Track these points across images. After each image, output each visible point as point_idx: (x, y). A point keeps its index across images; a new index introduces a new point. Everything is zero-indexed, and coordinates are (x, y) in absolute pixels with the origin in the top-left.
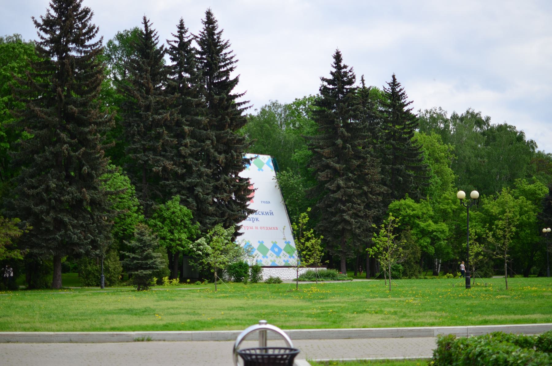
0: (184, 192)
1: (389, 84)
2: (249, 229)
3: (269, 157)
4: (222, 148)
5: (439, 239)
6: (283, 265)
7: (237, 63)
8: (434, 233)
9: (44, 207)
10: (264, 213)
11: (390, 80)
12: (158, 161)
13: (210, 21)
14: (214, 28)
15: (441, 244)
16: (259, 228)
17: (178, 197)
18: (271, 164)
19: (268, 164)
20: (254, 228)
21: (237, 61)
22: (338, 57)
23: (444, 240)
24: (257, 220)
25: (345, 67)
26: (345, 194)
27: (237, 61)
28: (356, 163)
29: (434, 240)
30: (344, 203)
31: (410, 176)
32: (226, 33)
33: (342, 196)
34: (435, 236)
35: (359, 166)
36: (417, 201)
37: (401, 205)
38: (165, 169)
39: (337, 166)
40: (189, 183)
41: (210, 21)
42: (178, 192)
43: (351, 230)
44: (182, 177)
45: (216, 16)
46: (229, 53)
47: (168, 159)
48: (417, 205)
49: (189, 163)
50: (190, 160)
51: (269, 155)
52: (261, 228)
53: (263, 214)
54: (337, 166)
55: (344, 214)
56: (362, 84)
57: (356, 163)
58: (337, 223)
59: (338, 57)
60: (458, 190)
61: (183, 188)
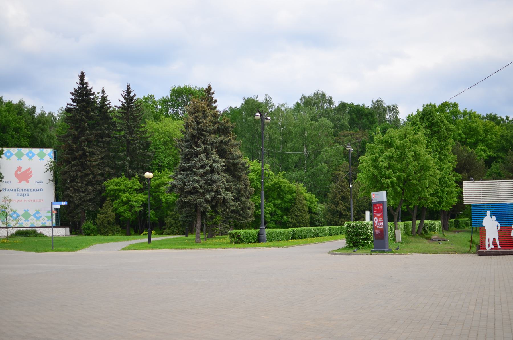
16: (27, 201)
24: (28, 195)
52: (29, 201)
53: (34, 190)
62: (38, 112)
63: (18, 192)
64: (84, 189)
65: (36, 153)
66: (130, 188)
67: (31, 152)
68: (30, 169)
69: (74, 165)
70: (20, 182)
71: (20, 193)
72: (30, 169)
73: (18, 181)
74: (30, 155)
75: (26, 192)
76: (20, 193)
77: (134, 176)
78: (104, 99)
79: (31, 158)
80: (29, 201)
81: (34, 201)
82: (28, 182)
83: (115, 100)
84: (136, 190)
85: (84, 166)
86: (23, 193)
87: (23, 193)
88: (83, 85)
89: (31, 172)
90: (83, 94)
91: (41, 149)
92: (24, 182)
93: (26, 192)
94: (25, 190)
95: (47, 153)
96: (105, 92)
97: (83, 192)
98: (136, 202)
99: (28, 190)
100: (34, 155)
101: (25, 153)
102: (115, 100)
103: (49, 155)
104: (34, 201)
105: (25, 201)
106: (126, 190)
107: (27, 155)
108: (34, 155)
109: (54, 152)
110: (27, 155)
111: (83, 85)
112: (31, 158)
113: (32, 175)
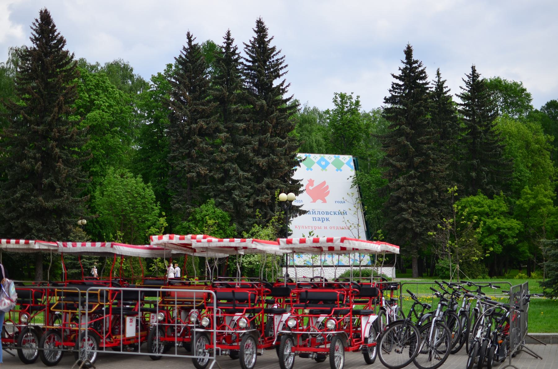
0: (222, 195)
1: (468, 76)
2: (317, 229)
3: (351, 157)
4: (265, 152)
5: (507, 237)
6: (302, 264)
7: (287, 68)
8: (501, 231)
9: (13, 214)
10: (337, 213)
11: (470, 71)
12: (194, 167)
13: (261, 29)
14: (265, 36)
15: (509, 242)
16: (328, 228)
17: (213, 201)
18: (352, 164)
19: (348, 163)
20: (323, 228)
21: (287, 66)
22: (409, 52)
23: (513, 237)
24: (327, 220)
25: (416, 62)
26: (406, 192)
27: (287, 66)
28: (417, 160)
29: (502, 238)
30: (406, 201)
31: (483, 170)
32: (276, 39)
33: (403, 194)
34: (503, 233)
35: (422, 162)
36: (491, 197)
37: (468, 201)
38: (199, 174)
39: (398, 164)
40: (227, 187)
41: (261, 29)
42: (215, 196)
43: (412, 228)
44: (222, 181)
45: (267, 24)
46: (281, 59)
47: (204, 166)
48: (489, 201)
49: (226, 167)
50: (227, 165)
51: (350, 155)
52: (331, 228)
53: (335, 213)
54: (398, 164)
55: (404, 213)
56: (437, 78)
57: (417, 160)
58: (399, 222)
59: (409, 52)
60: (280, 193)
61: (222, 192)
62: (301, 108)
63: (314, 216)
64: (426, 212)
65: (330, 161)
66: (495, 210)
67: (323, 159)
68: (324, 183)
69: (411, 177)
70: (314, 201)
71: (317, 216)
72: (324, 183)
73: (312, 200)
74: (323, 163)
75: (325, 216)
76: (317, 216)
77: (498, 194)
78: (440, 86)
79: (324, 168)
80: (331, 228)
81: (337, 228)
82: (325, 201)
83: (456, 89)
84: (502, 213)
85: (424, 177)
86: (321, 216)
87: (321, 216)
88: (411, 65)
89: (327, 187)
90: (411, 75)
91: (337, 156)
92: (319, 201)
93: (325, 216)
94: (323, 213)
95: (345, 162)
96: (441, 76)
97: (425, 216)
98: (509, 229)
99: (327, 213)
100: (327, 163)
101: (316, 161)
102: (456, 89)
103: (348, 163)
104: (337, 228)
105: (325, 228)
106: (490, 213)
107: (319, 163)
108: (327, 163)
109: (354, 160)
110: (319, 163)
111: (411, 65)
112: (324, 168)
113: (329, 192)
